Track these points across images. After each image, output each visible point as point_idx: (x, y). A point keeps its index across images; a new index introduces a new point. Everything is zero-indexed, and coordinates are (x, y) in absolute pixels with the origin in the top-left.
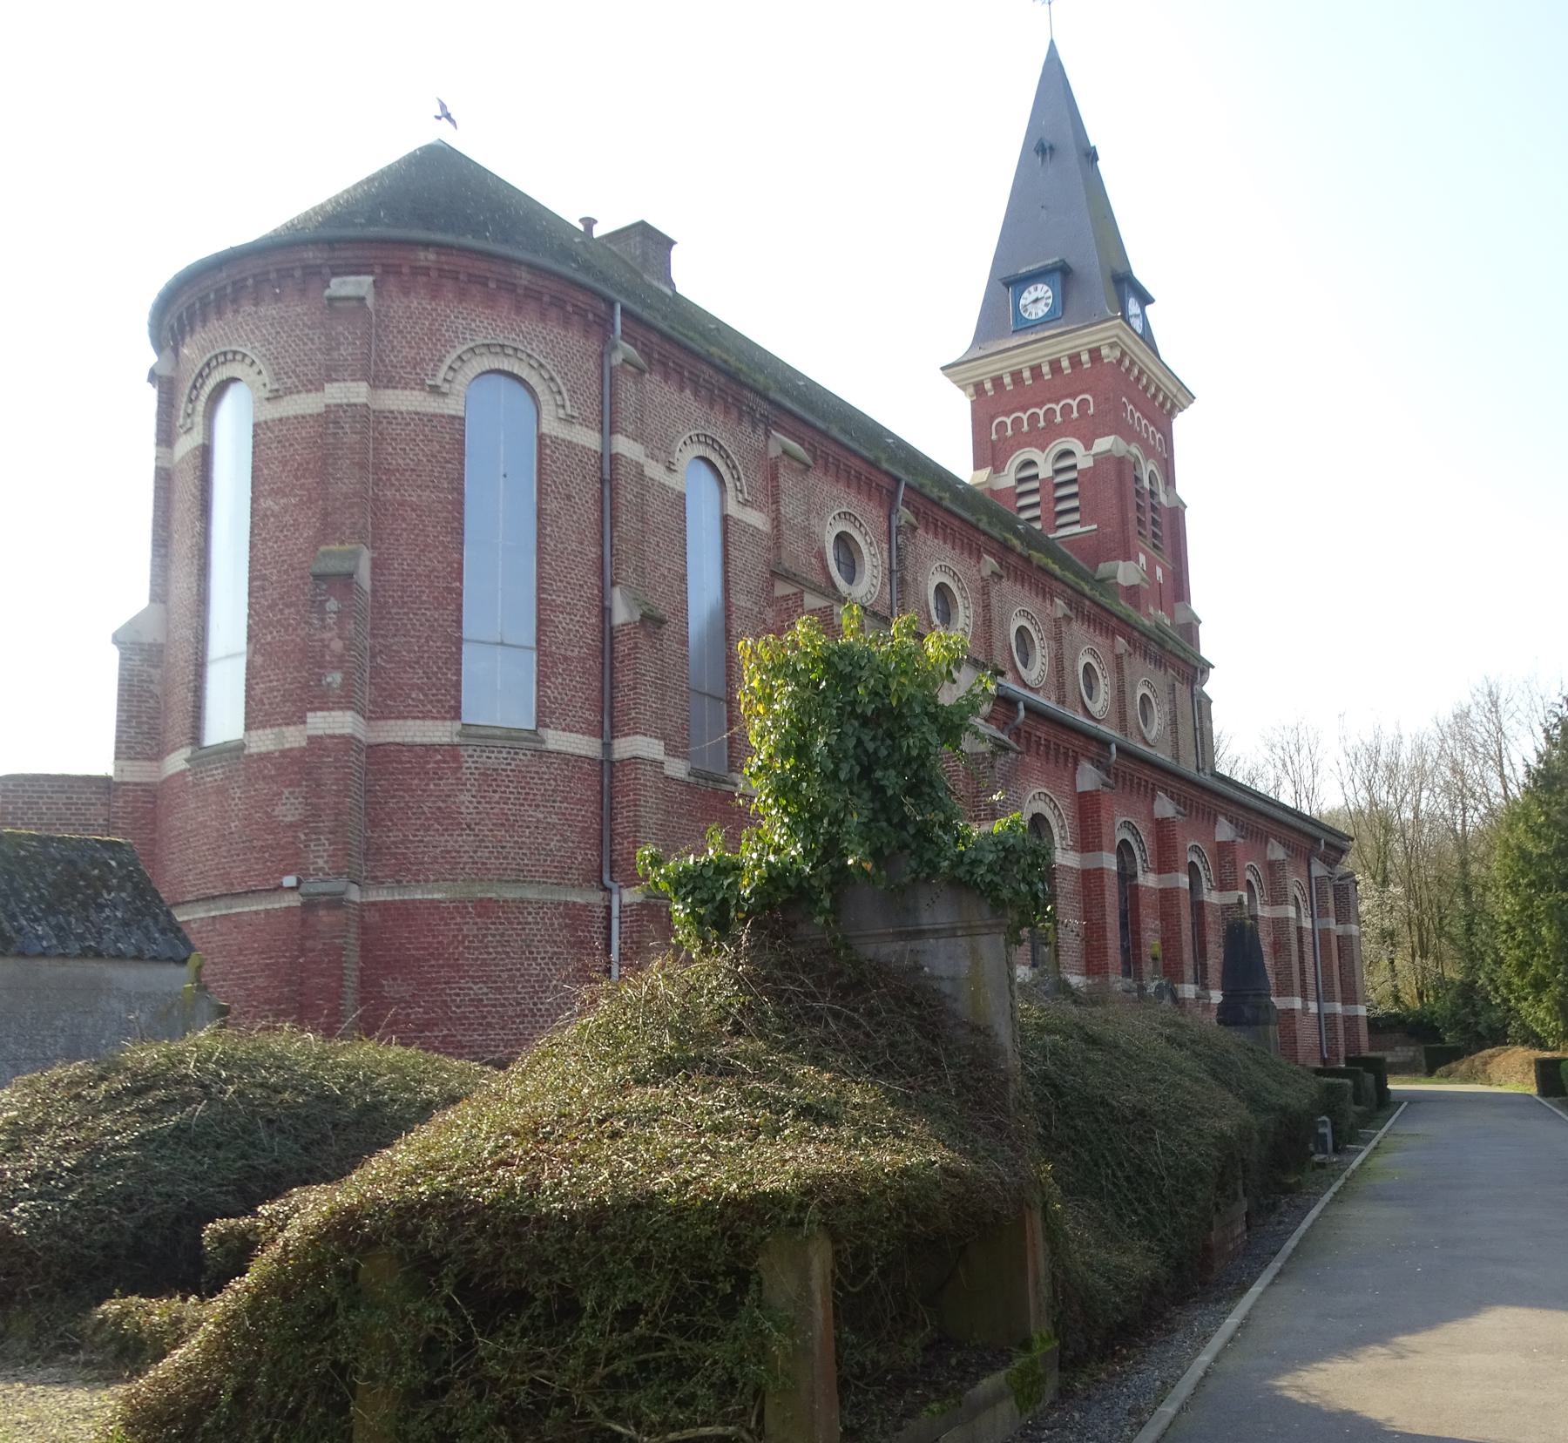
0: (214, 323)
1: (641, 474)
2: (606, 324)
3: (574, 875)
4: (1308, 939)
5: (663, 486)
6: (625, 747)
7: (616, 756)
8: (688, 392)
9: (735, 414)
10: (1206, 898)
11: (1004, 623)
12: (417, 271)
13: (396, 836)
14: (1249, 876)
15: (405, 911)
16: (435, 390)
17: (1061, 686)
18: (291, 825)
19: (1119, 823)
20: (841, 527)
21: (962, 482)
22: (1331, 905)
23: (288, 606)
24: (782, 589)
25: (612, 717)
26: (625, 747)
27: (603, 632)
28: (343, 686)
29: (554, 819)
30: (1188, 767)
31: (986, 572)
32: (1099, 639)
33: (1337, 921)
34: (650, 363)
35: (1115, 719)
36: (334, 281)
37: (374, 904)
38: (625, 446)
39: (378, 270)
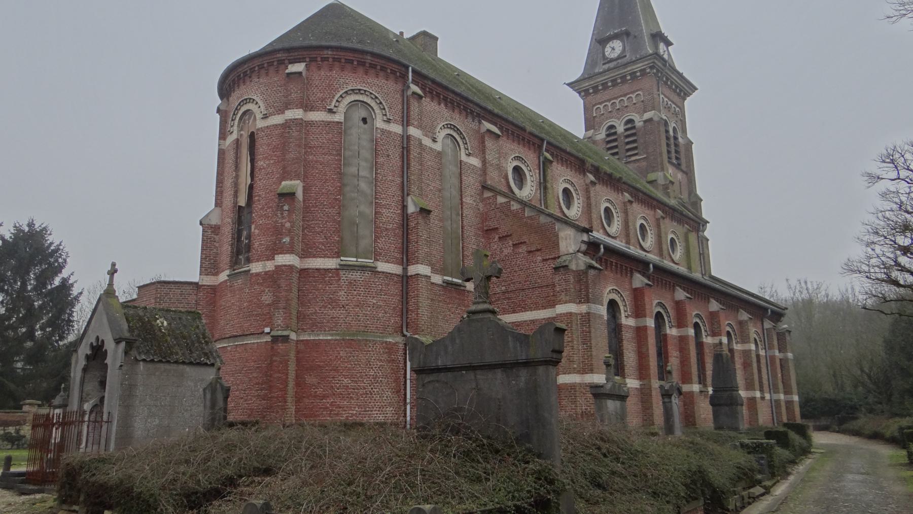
0: (242, 87)
1: (421, 143)
2: (404, 77)
3: (390, 329)
4: (763, 361)
5: (431, 149)
6: (413, 270)
7: (409, 274)
8: (442, 105)
9: (465, 113)
10: (704, 340)
11: (598, 205)
12: (324, 59)
13: (311, 310)
14: (728, 329)
15: (317, 344)
16: (330, 111)
17: (627, 236)
18: (268, 305)
19: (653, 303)
20: (516, 163)
21: (576, 138)
22: (775, 343)
23: (268, 208)
24: (487, 194)
25: (407, 256)
26: (413, 270)
27: (403, 216)
28: (289, 244)
29: (381, 303)
30: (697, 275)
31: (588, 181)
32: (648, 212)
33: (780, 351)
34: (425, 93)
35: (656, 251)
36: (290, 66)
37: (302, 341)
38: (413, 131)
39: (308, 60)
